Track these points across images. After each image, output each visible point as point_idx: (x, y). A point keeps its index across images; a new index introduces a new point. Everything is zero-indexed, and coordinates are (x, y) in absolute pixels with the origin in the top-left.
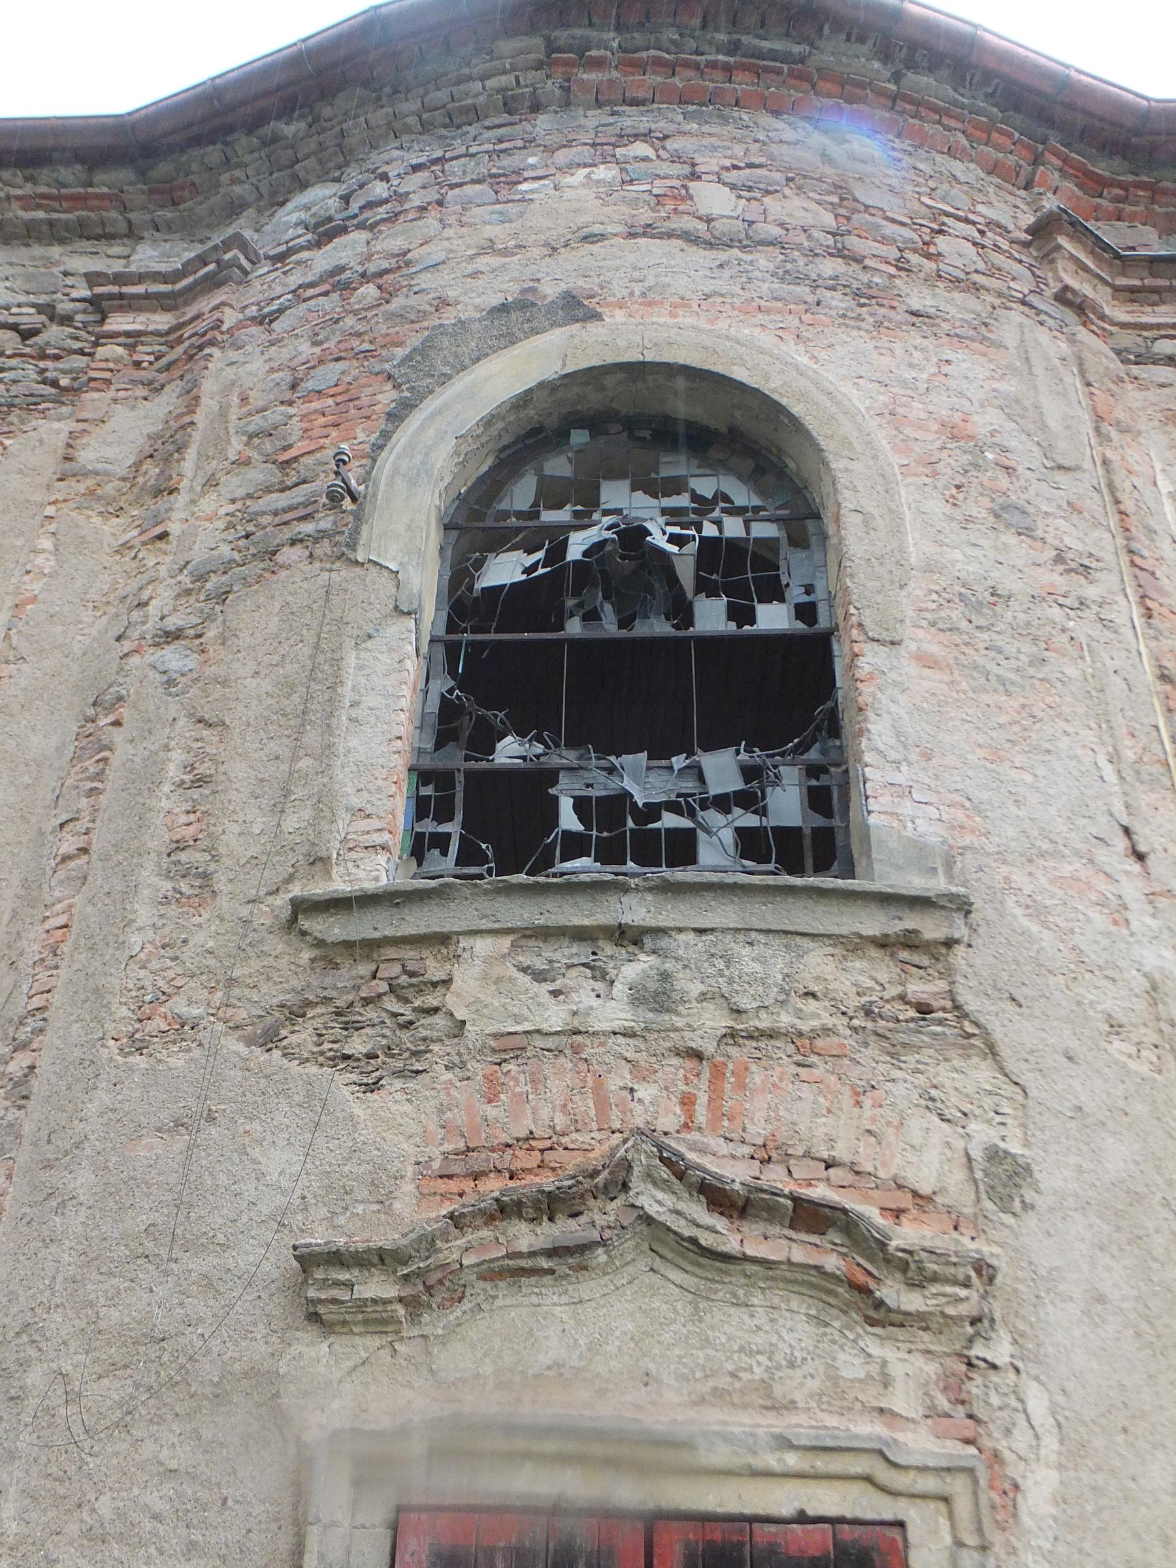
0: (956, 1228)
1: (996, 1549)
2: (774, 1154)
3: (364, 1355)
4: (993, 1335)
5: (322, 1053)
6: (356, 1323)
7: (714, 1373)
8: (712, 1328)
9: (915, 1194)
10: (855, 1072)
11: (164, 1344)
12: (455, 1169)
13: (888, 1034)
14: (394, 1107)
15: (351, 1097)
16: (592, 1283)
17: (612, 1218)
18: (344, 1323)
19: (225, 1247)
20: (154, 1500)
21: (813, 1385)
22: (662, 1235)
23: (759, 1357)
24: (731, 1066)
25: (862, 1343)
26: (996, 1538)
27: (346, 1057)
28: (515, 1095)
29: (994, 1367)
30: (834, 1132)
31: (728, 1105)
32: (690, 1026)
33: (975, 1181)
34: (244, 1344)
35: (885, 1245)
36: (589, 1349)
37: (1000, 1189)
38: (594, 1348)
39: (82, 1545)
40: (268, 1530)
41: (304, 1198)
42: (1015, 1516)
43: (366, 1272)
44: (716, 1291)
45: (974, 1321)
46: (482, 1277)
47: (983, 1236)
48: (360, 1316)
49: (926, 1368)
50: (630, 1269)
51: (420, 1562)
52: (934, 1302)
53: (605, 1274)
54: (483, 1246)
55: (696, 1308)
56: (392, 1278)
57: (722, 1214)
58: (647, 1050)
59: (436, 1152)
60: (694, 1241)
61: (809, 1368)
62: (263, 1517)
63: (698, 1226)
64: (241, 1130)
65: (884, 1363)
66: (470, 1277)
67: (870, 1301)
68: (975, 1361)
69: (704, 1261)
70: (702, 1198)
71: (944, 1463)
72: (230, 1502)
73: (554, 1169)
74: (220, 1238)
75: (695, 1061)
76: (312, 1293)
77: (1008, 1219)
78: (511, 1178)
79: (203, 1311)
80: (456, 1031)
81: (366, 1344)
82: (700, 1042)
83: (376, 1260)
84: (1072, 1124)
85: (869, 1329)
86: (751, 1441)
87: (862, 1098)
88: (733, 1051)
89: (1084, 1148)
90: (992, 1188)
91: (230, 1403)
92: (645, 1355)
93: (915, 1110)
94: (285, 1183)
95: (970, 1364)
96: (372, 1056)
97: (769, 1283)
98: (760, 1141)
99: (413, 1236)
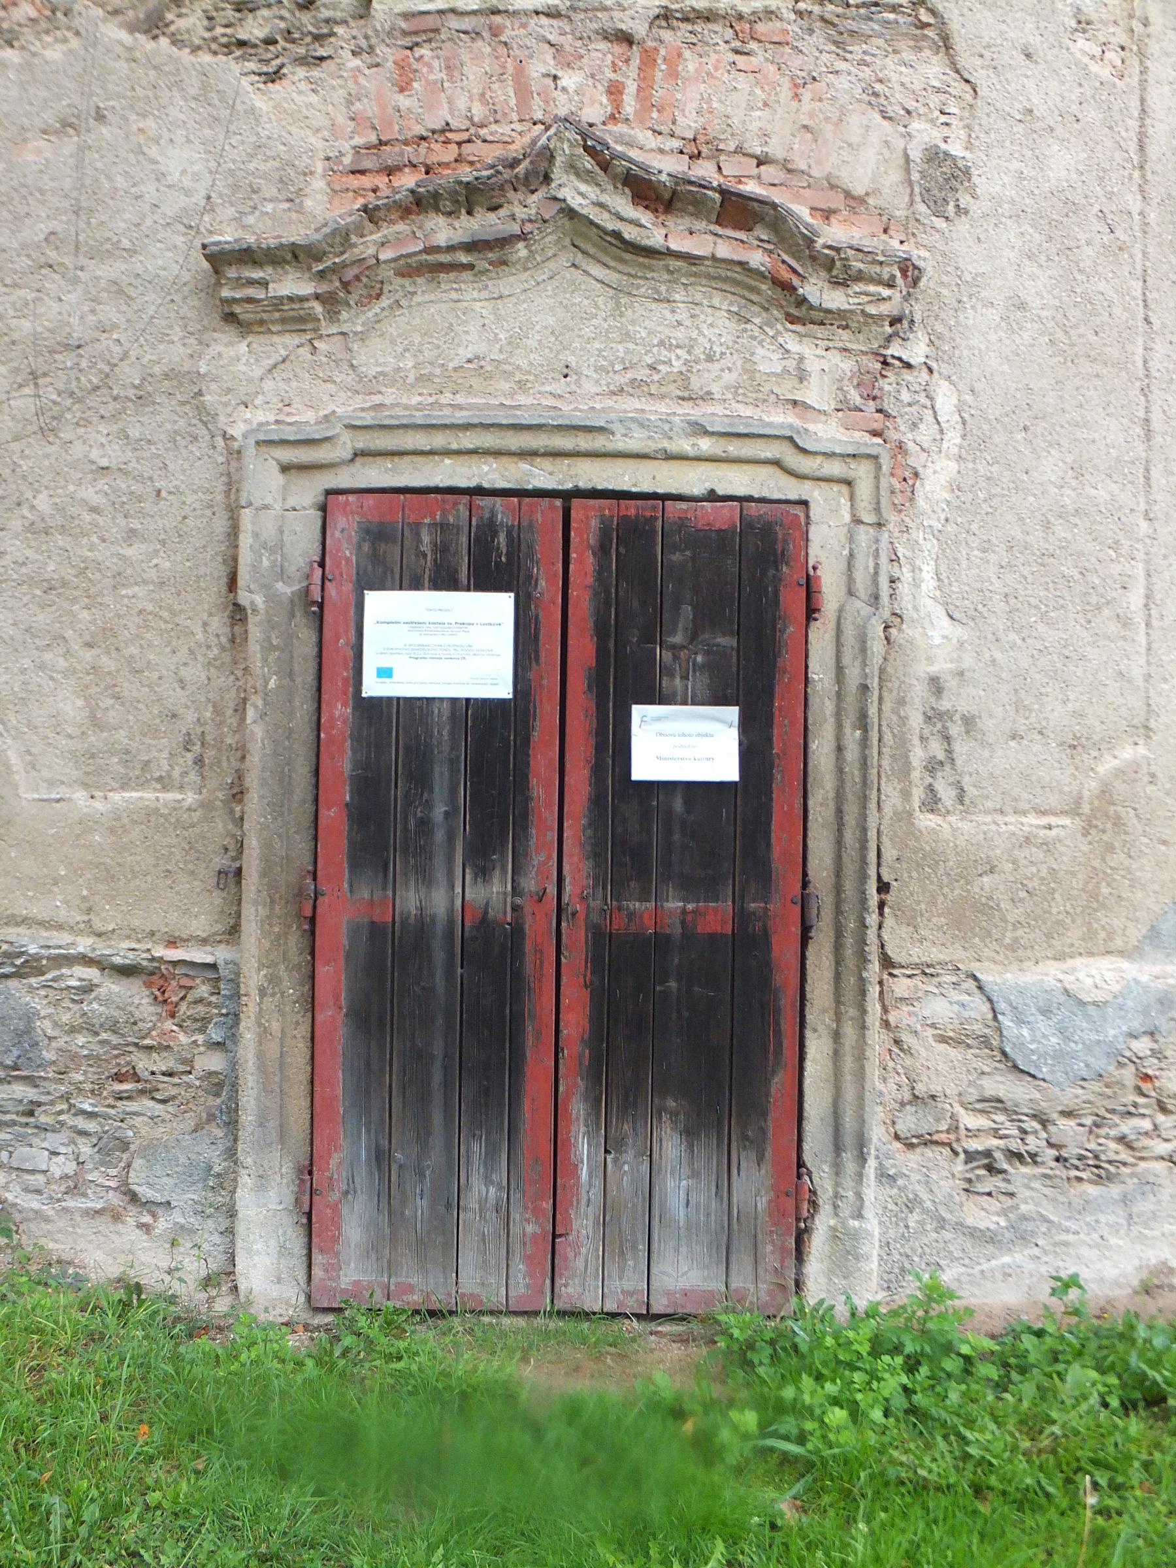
0: (885, 231)
1: (891, 526)
2: (704, 150)
3: (284, 353)
4: (911, 336)
5: (215, 39)
6: (272, 322)
7: (633, 366)
8: (633, 322)
9: (848, 194)
10: (796, 62)
11: (80, 351)
12: (367, 164)
13: (836, 20)
14: (298, 98)
15: (250, 89)
16: (512, 279)
17: (533, 211)
18: (261, 322)
19: (132, 252)
20: (90, 494)
21: (729, 378)
22: (584, 229)
23: (679, 351)
24: (663, 52)
25: (781, 340)
26: (892, 517)
27: (242, 44)
28: (428, 83)
29: (908, 366)
30: (769, 127)
31: (658, 95)
32: (620, 5)
33: (910, 183)
34: (161, 347)
35: (813, 241)
36: (510, 343)
37: (935, 192)
38: (514, 342)
39: (27, 539)
40: (202, 516)
41: (209, 198)
42: (911, 500)
43: (280, 271)
44: (638, 287)
45: (895, 321)
46: (400, 274)
47: (912, 240)
48: (277, 315)
49: (842, 365)
50: (551, 264)
51: (350, 537)
52: (856, 301)
53: (526, 269)
54: (399, 240)
55: (618, 304)
56: (307, 275)
57: (646, 207)
58: (573, 32)
59: (346, 146)
60: (617, 235)
61: (727, 361)
62: (197, 505)
63: (622, 219)
64: (135, 127)
65: (802, 359)
66: (387, 272)
67: (792, 299)
68: (890, 360)
69: (628, 256)
70: (627, 190)
71: (851, 451)
72: (164, 494)
73: (471, 163)
74: (126, 243)
75: (625, 46)
76: (226, 293)
77: (940, 223)
78: (427, 173)
79: (114, 316)
80: (362, 11)
81: (285, 343)
82: (631, 23)
83: (289, 257)
84: (1020, 128)
85: (789, 326)
86: (667, 427)
87: (801, 90)
88: (666, 35)
89: (1029, 154)
90: (928, 191)
91: (154, 403)
92: (565, 349)
93: (856, 106)
94: (187, 182)
95: (885, 363)
96: (270, 41)
97: (692, 279)
98: (690, 135)
99: (326, 230)
